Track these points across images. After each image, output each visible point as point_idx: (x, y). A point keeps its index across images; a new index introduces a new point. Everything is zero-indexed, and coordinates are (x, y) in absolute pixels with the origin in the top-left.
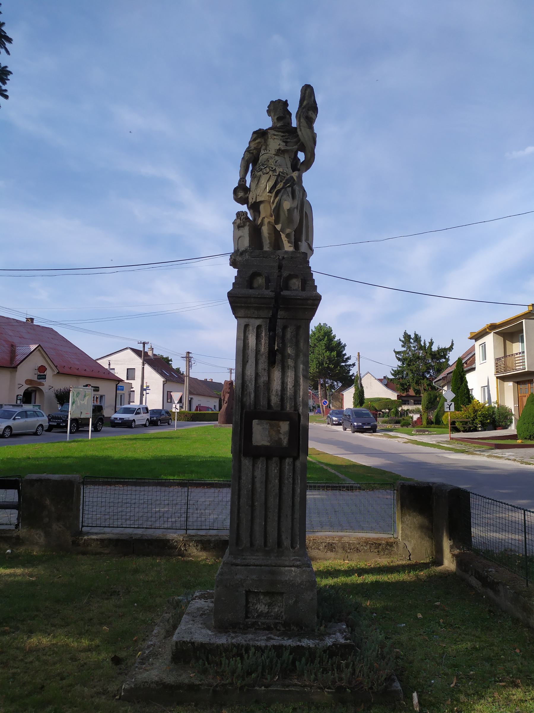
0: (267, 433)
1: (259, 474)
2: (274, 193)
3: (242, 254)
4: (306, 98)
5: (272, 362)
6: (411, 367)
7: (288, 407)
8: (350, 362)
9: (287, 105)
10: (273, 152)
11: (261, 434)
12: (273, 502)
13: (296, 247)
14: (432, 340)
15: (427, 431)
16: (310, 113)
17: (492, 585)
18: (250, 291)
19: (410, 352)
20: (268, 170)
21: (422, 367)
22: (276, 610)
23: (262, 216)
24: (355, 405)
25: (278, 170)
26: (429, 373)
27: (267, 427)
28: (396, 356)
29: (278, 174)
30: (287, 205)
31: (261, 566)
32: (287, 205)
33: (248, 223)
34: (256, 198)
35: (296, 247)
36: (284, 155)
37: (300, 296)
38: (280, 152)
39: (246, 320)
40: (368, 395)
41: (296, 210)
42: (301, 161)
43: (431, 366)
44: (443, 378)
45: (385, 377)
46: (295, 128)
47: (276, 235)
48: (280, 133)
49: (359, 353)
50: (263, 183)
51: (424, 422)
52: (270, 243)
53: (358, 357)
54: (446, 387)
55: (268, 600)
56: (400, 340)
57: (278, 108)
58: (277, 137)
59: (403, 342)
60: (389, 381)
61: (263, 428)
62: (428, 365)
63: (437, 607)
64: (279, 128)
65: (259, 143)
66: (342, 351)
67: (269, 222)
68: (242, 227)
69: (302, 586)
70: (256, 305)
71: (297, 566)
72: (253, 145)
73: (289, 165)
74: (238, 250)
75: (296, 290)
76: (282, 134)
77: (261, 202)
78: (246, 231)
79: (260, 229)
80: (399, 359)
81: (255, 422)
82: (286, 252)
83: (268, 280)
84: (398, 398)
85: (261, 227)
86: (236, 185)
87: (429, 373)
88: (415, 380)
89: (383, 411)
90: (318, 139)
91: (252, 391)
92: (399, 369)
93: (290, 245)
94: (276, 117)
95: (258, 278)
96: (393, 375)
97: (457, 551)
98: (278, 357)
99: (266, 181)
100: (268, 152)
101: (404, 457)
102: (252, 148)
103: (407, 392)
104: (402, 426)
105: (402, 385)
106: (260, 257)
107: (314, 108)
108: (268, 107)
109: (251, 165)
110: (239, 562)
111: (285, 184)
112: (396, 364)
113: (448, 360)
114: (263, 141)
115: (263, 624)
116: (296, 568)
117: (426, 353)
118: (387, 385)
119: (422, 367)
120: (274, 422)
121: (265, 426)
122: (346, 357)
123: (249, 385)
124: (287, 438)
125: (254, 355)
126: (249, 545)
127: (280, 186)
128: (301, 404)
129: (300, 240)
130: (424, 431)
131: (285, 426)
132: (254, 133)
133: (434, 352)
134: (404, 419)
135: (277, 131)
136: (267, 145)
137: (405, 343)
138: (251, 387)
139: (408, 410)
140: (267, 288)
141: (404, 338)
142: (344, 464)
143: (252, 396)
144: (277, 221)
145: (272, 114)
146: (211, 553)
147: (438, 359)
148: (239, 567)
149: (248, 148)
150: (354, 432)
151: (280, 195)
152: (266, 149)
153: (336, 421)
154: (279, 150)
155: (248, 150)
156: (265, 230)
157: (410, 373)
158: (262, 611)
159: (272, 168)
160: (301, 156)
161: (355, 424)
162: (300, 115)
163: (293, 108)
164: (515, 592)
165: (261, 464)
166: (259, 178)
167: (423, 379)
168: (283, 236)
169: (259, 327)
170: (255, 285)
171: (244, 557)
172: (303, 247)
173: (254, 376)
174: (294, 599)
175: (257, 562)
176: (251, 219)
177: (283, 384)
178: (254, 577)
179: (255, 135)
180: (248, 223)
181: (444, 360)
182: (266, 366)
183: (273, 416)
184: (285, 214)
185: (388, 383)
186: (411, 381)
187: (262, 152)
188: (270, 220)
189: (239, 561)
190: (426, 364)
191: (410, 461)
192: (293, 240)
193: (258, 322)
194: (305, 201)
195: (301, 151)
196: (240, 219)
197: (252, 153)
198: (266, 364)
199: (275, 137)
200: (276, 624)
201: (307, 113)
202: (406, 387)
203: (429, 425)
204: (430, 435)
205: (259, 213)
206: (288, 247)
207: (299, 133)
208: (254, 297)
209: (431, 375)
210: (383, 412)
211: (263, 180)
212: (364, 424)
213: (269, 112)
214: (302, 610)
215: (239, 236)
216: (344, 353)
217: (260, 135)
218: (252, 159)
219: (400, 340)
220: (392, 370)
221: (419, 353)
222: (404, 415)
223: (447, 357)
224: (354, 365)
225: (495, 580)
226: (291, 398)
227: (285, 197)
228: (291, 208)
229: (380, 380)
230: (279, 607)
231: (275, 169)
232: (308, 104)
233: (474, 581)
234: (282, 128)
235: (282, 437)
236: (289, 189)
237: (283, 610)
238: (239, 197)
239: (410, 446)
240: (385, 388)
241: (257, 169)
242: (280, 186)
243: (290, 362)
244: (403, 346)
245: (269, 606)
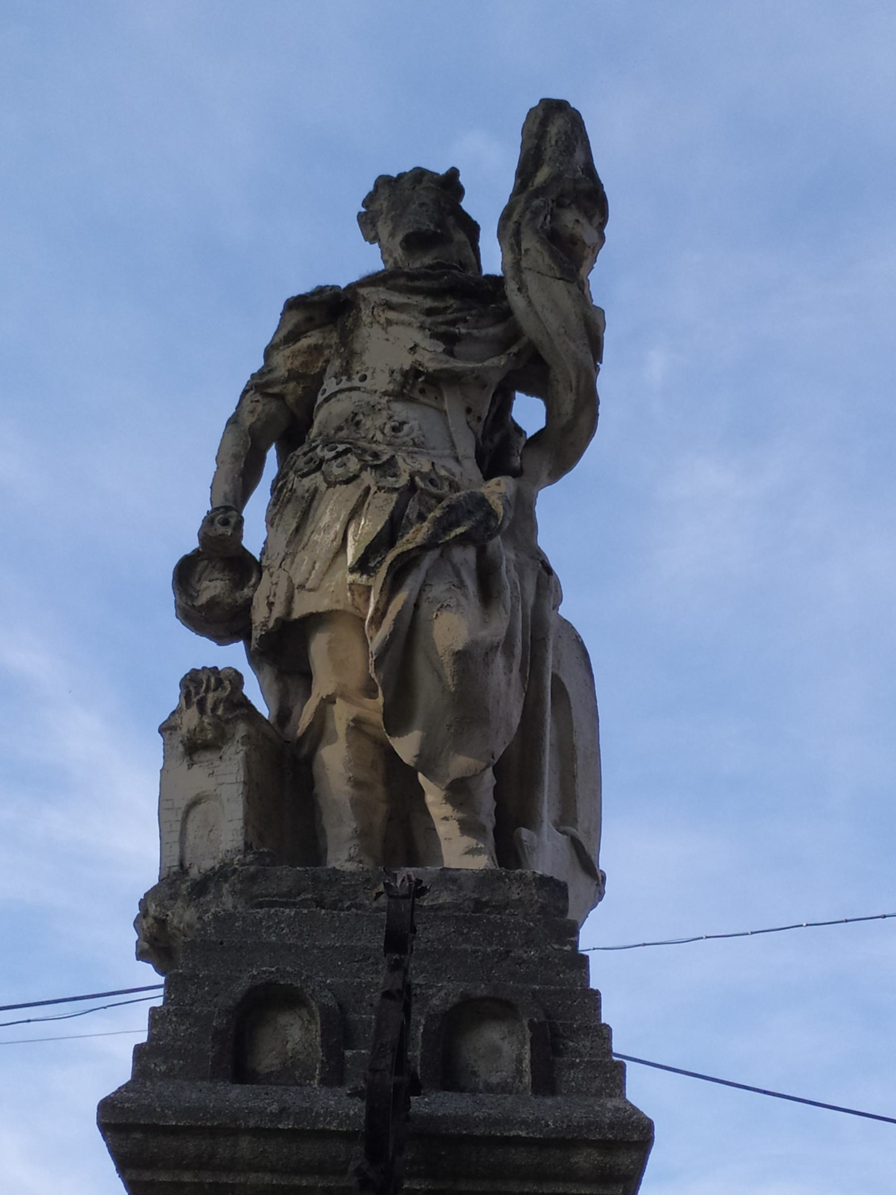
2: (383, 571)
3: (201, 887)
4: (549, 153)
9: (460, 192)
10: (382, 382)
13: (508, 852)
16: (569, 218)
18: (236, 1095)
20: (353, 464)
23: (324, 683)
25: (405, 466)
29: (404, 480)
30: (451, 628)
32: (451, 628)
33: (241, 729)
34: (290, 600)
35: (508, 852)
36: (439, 396)
37: (524, 1123)
38: (414, 384)
41: (499, 661)
42: (528, 436)
46: (497, 282)
47: (398, 784)
48: (415, 299)
50: (328, 527)
52: (362, 834)
57: (418, 211)
58: (404, 317)
64: (411, 277)
65: (316, 349)
67: (357, 725)
68: (208, 746)
70: (267, 1178)
72: (283, 363)
73: (467, 446)
74: (183, 870)
75: (504, 1088)
76: (429, 303)
77: (315, 621)
78: (226, 778)
79: (309, 761)
82: (449, 878)
83: (338, 1031)
86: (191, 544)
90: (608, 338)
93: (469, 841)
94: (399, 237)
95: (284, 1019)
99: (344, 515)
100: (356, 383)
102: (281, 372)
106: (304, 903)
107: (592, 200)
108: (365, 204)
109: (272, 454)
111: (444, 525)
114: (334, 338)
127: (415, 536)
129: (530, 820)
132: (294, 304)
135: (400, 290)
136: (352, 354)
140: (335, 1075)
144: (398, 717)
145: (384, 230)
149: (261, 373)
151: (412, 582)
152: (346, 371)
154: (415, 373)
155: (259, 386)
156: (335, 761)
159: (376, 455)
160: (529, 413)
162: (518, 224)
163: (487, 198)
166: (311, 501)
168: (434, 797)
170: (267, 1059)
172: (547, 854)
176: (263, 709)
179: (296, 317)
180: (241, 729)
184: (440, 678)
187: (330, 385)
188: (364, 713)
192: (489, 823)
194: (552, 620)
195: (530, 391)
196: (201, 704)
197: (280, 397)
199: (392, 315)
201: (554, 217)
205: (307, 676)
206: (459, 850)
207: (517, 301)
208: (257, 1132)
211: (330, 514)
213: (368, 221)
215: (191, 795)
217: (323, 313)
218: (278, 422)
227: (438, 590)
228: (474, 644)
231: (392, 461)
232: (556, 178)
234: (426, 276)
236: (466, 556)
238: (203, 599)
241: (301, 463)
242: (415, 536)
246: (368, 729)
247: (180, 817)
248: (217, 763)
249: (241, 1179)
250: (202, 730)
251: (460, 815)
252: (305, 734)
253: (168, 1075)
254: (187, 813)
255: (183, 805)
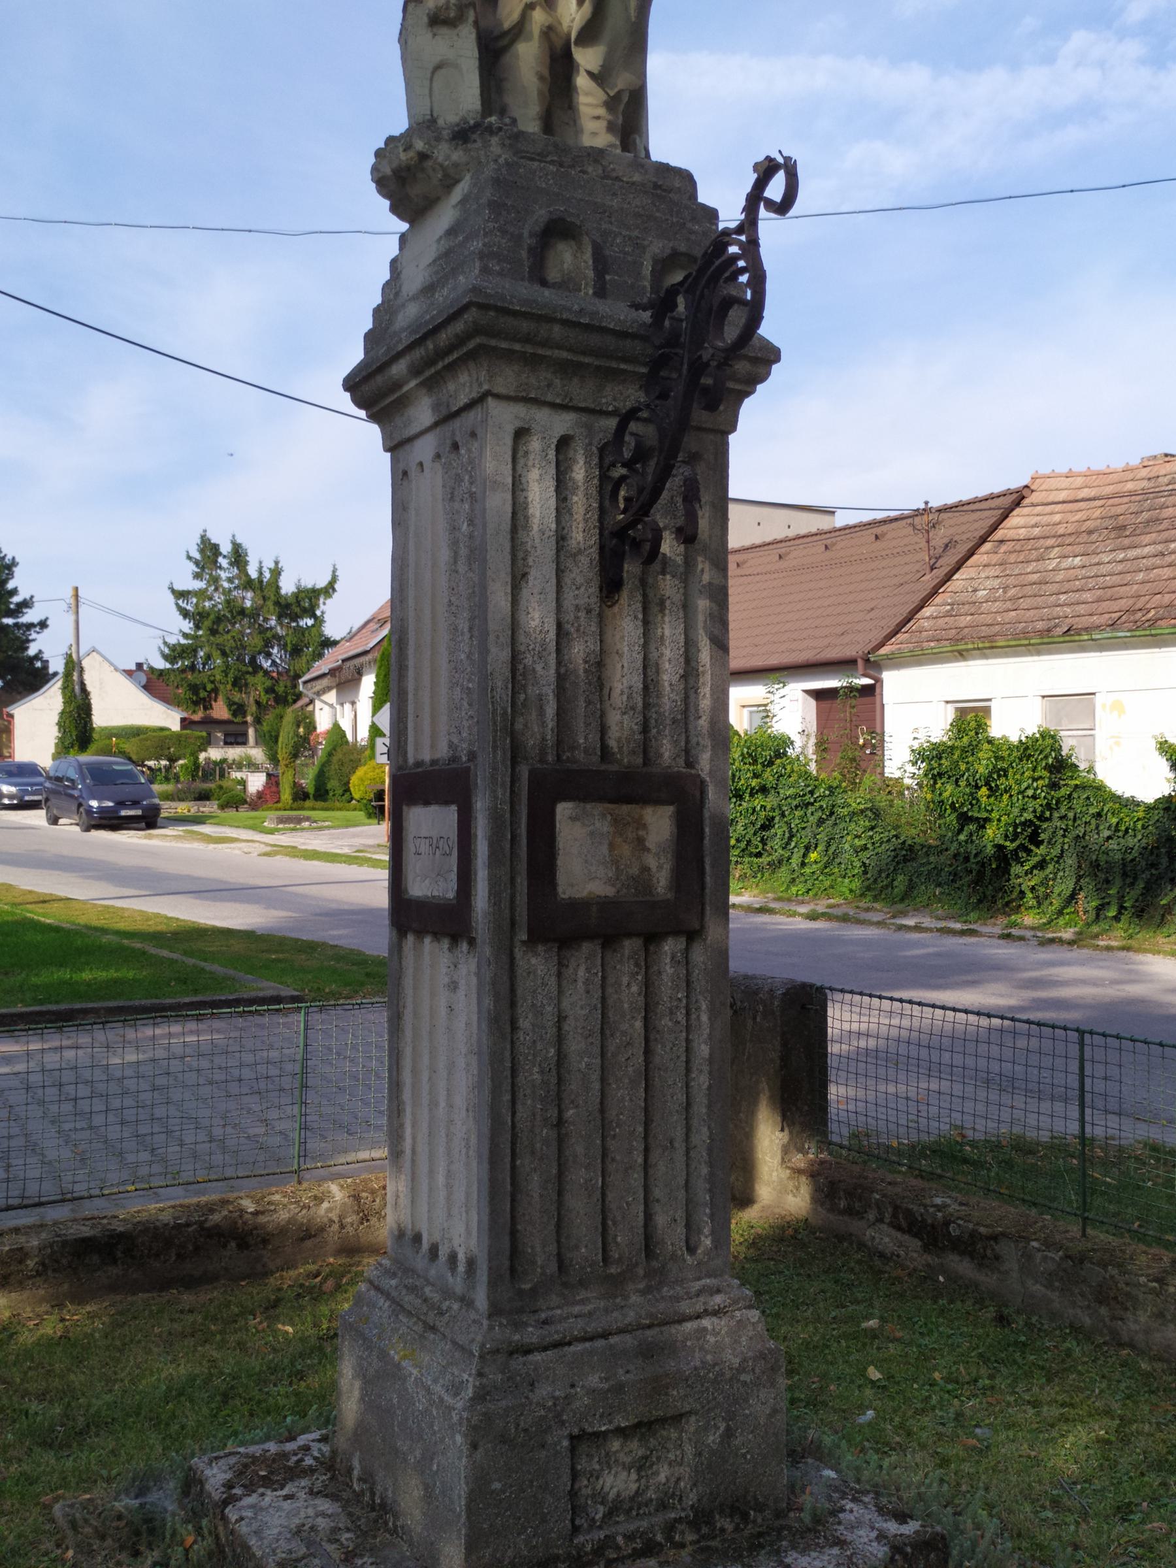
0: (605, 849)
1: (578, 1002)
5: (610, 586)
6: (219, 639)
7: (667, 751)
8: (30, 616)
11: (587, 857)
12: (626, 1098)
14: (277, 563)
15: (308, 819)
17: (974, 1246)
19: (216, 595)
21: (254, 641)
22: (662, 1478)
24: (63, 748)
26: (268, 655)
27: (604, 826)
28: (177, 604)
31: (605, 1335)
39: (520, 410)
40: (103, 716)
43: (277, 637)
44: (332, 672)
45: (139, 666)
49: (77, 589)
51: (286, 795)
53: (72, 601)
54: (334, 692)
55: (636, 1448)
56: (189, 558)
59: (197, 563)
60: (154, 677)
61: (592, 834)
62: (269, 634)
63: (873, 1334)
66: (5, 581)
69: (743, 1377)
70: (565, 355)
71: (717, 1313)
80: (185, 614)
81: (563, 810)
84: (183, 727)
85: (513, 41)
87: (268, 655)
88: (231, 675)
89: (151, 763)
91: (549, 692)
92: (183, 641)
96: (166, 657)
97: (799, 1160)
98: (631, 568)
101: (296, 895)
103: (205, 708)
104: (222, 807)
105: (194, 688)
110: (534, 1340)
112: (178, 628)
113: (319, 621)
115: (630, 1538)
116: (715, 1319)
117: (264, 598)
118: (148, 688)
119: (254, 641)
120: (625, 808)
121: (598, 825)
122: (16, 599)
123: (539, 668)
124: (667, 867)
125: (550, 553)
126: (553, 1268)
128: (707, 742)
130: (299, 820)
131: (659, 823)
133: (286, 597)
134: (221, 787)
137: (203, 568)
138: (546, 674)
139: (224, 761)
141: (202, 551)
142: (162, 928)
143: (551, 710)
146: (26, 1294)
147: (295, 618)
148: (537, 1357)
150: (87, 829)
153: (11, 797)
157: (216, 654)
158: (618, 1495)
161: (94, 804)
164: (1068, 1257)
165: (583, 964)
167: (255, 673)
169: (564, 443)
171: (543, 1316)
173: (552, 635)
174: (722, 1426)
175: (593, 1327)
177: (649, 669)
178: (594, 1380)
181: (310, 622)
182: (594, 600)
183: (624, 785)
184: (627, 9)
185: (154, 683)
186: (218, 677)
189: (532, 1334)
190: (262, 630)
191: (346, 907)
193: (562, 423)
198: (594, 589)
200: (670, 1528)
202: (203, 694)
203: (300, 803)
204: (320, 829)
208: (566, 323)
209: (274, 663)
210: (150, 768)
212: (121, 804)
214: (744, 1456)
216: (10, 585)
219: (189, 558)
220: (165, 643)
221: (244, 598)
222: (213, 774)
223: (318, 613)
224: (43, 625)
225: (982, 1230)
226: (674, 721)
229: (129, 673)
230: (670, 1464)
233: (885, 1238)
235: (652, 862)
237: (685, 1471)
239: (282, 863)
240: (144, 698)
243: (669, 587)
244: (197, 576)
245: (640, 1469)
246: (553, 35)
247: (429, 76)
248: (455, 38)
249: (548, 353)
250: (448, 8)
251: (610, 117)
252: (510, 30)
253: (500, 274)
254: (433, 73)
255: (430, 67)
